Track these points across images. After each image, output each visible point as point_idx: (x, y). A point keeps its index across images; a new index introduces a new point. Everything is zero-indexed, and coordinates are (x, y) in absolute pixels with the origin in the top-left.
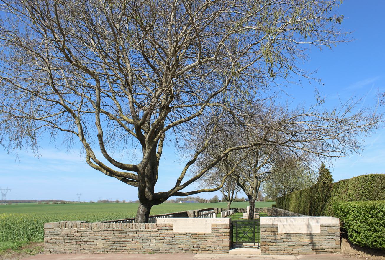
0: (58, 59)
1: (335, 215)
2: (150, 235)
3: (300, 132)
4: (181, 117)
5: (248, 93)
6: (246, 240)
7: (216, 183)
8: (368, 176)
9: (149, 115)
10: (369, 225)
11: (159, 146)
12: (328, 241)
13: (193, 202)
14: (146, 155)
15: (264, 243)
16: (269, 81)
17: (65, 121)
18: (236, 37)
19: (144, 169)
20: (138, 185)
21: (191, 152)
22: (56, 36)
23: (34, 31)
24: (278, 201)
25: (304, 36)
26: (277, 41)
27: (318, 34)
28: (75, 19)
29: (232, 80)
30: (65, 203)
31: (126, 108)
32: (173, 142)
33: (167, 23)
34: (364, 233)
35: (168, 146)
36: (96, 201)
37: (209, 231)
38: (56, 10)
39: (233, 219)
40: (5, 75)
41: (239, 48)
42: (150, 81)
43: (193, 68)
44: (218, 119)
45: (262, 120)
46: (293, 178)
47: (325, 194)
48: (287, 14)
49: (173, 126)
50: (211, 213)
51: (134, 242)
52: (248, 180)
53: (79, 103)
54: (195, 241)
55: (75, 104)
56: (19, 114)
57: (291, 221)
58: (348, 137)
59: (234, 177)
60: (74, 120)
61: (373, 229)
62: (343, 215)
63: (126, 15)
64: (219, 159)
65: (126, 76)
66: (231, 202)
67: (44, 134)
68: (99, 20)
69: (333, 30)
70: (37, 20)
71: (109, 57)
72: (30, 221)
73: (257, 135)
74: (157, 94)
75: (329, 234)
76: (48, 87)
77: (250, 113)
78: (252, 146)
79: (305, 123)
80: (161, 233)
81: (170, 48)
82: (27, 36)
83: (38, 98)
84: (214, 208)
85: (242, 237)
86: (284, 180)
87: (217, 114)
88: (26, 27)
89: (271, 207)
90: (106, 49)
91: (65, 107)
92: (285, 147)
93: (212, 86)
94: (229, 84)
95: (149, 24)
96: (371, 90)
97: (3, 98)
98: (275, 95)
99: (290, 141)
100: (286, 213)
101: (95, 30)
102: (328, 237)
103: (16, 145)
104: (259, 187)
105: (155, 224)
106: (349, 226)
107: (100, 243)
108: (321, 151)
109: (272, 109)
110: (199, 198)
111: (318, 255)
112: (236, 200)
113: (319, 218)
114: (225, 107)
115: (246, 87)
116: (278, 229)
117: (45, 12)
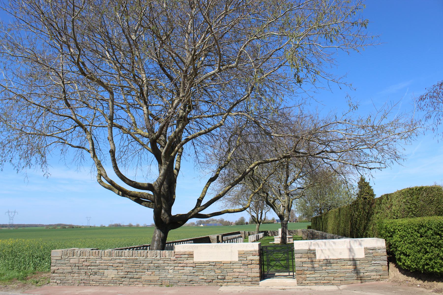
0: (72, 72)
1: (380, 236)
2: (167, 265)
3: (335, 142)
4: (201, 128)
5: (274, 100)
6: (279, 269)
7: (242, 202)
8: (413, 189)
9: (165, 128)
10: (418, 246)
11: (177, 161)
12: (374, 267)
13: (215, 226)
14: (162, 172)
15: (300, 272)
16: (295, 87)
17: (77, 137)
18: (258, 43)
19: (160, 187)
20: (154, 206)
21: (212, 167)
22: (72, 50)
23: (50, 47)
24: (314, 221)
25: (329, 40)
26: (302, 46)
27: (344, 38)
28: (91, 33)
29: (255, 87)
30: (73, 228)
31: (141, 121)
32: (192, 157)
33: (185, 32)
34: (413, 256)
35: (187, 161)
36: (107, 225)
37: (236, 259)
38: (73, 25)
39: (263, 244)
40: (20, 91)
41: (262, 54)
42: (167, 91)
43: (213, 76)
44: (242, 129)
45: (290, 129)
46: (329, 194)
47: (367, 211)
48: (310, 19)
49: (192, 139)
50: (237, 238)
51: (150, 273)
52: (279, 197)
53: (92, 117)
54: (220, 271)
55: (87, 118)
56: (30, 130)
57: (331, 245)
58: (386, 146)
59: (262, 195)
60: (86, 136)
61: (423, 250)
62: (389, 235)
63: (142, 26)
64: (244, 172)
65: (141, 87)
66: (260, 224)
67: (54, 151)
68: (116, 33)
69: (359, 33)
70: (54, 36)
71: (124, 68)
72: (36, 247)
73: (285, 146)
74: (174, 105)
75: (374, 259)
76: (61, 101)
77: (277, 122)
78: (281, 159)
79: (338, 132)
80: (180, 262)
81: (187, 56)
82: (44, 51)
83: (50, 113)
84: (240, 232)
85: (274, 266)
86: (319, 196)
87: (240, 124)
88: (41, 42)
89: (307, 229)
90: (121, 61)
91: (77, 121)
92: (319, 159)
93: (234, 94)
94: (253, 92)
95: (166, 33)
96: (406, 94)
97: (17, 115)
98: (303, 101)
99: (323, 152)
100: (324, 235)
101: (111, 42)
102: (373, 262)
103: (25, 163)
104: (292, 206)
105: (173, 251)
106: (396, 248)
107: (111, 274)
108: (359, 163)
109: (301, 117)
110: (223, 220)
111: (363, 284)
112: (265, 222)
113: (362, 240)
114: (249, 116)
115: (271, 94)
116: (315, 255)
117: (62, 28)
